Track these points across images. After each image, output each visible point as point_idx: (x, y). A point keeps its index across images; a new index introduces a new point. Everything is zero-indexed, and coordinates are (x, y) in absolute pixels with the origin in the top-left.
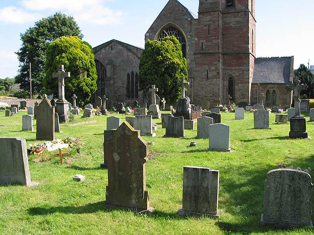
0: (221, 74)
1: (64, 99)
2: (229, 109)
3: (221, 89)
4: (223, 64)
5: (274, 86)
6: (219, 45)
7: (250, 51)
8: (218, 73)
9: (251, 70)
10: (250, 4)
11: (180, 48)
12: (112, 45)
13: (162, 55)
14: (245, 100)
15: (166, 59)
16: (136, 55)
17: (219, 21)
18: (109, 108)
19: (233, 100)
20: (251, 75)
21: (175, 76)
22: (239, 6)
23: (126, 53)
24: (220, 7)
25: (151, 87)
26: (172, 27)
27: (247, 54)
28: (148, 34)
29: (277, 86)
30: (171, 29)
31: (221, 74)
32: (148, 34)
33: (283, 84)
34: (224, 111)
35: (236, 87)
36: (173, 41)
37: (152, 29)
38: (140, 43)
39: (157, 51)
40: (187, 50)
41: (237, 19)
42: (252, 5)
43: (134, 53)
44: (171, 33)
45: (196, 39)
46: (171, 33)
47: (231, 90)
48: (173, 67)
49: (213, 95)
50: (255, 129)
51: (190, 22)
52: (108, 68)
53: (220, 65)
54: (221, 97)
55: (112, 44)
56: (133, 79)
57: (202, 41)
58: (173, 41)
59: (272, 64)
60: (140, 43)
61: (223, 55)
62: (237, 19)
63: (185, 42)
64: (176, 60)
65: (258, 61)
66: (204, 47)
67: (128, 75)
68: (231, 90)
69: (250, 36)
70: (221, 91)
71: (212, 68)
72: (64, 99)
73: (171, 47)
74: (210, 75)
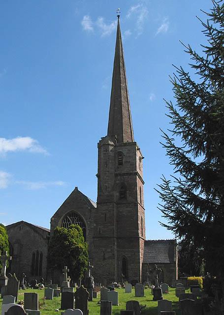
0: (116, 255)
1: (5, 275)
2: (122, 286)
3: (116, 269)
4: (118, 246)
5: (161, 265)
6: (114, 231)
7: (140, 235)
8: (114, 254)
9: (141, 251)
10: (139, 197)
11: (82, 234)
12: (21, 225)
13: (69, 241)
14: (136, 279)
15: (71, 244)
16: (43, 237)
17: (113, 210)
18: (27, 286)
19: (126, 278)
20: (141, 256)
21: (78, 257)
22: (130, 199)
23: (28, 228)
24: (115, 199)
25: (64, 268)
26: (75, 213)
27: (137, 238)
28: (53, 219)
29: (163, 265)
30: (73, 215)
31: (116, 255)
32: (53, 219)
33: (168, 263)
34: (118, 287)
35: (129, 267)
36: (78, 229)
37: (57, 215)
38: (45, 224)
39: (65, 237)
40: (87, 234)
41: (128, 209)
42: (141, 200)
43: (41, 234)
44: (73, 219)
45: (95, 225)
46: (73, 219)
47: (125, 269)
48: (77, 251)
49: (109, 273)
50: (126, 293)
51: (90, 211)
52: (16, 245)
53: (115, 247)
54: (116, 275)
55: (22, 224)
56: (37, 258)
57: (99, 227)
58: (78, 229)
59: (160, 246)
60: (45, 224)
61: (118, 238)
62: (128, 209)
63: (85, 227)
64: (81, 245)
65: (148, 243)
66: (101, 232)
67: (34, 254)
68: (125, 269)
69: (139, 222)
70: (116, 270)
71: (108, 250)
72: (5, 275)
73: (75, 234)
74: (106, 256)
